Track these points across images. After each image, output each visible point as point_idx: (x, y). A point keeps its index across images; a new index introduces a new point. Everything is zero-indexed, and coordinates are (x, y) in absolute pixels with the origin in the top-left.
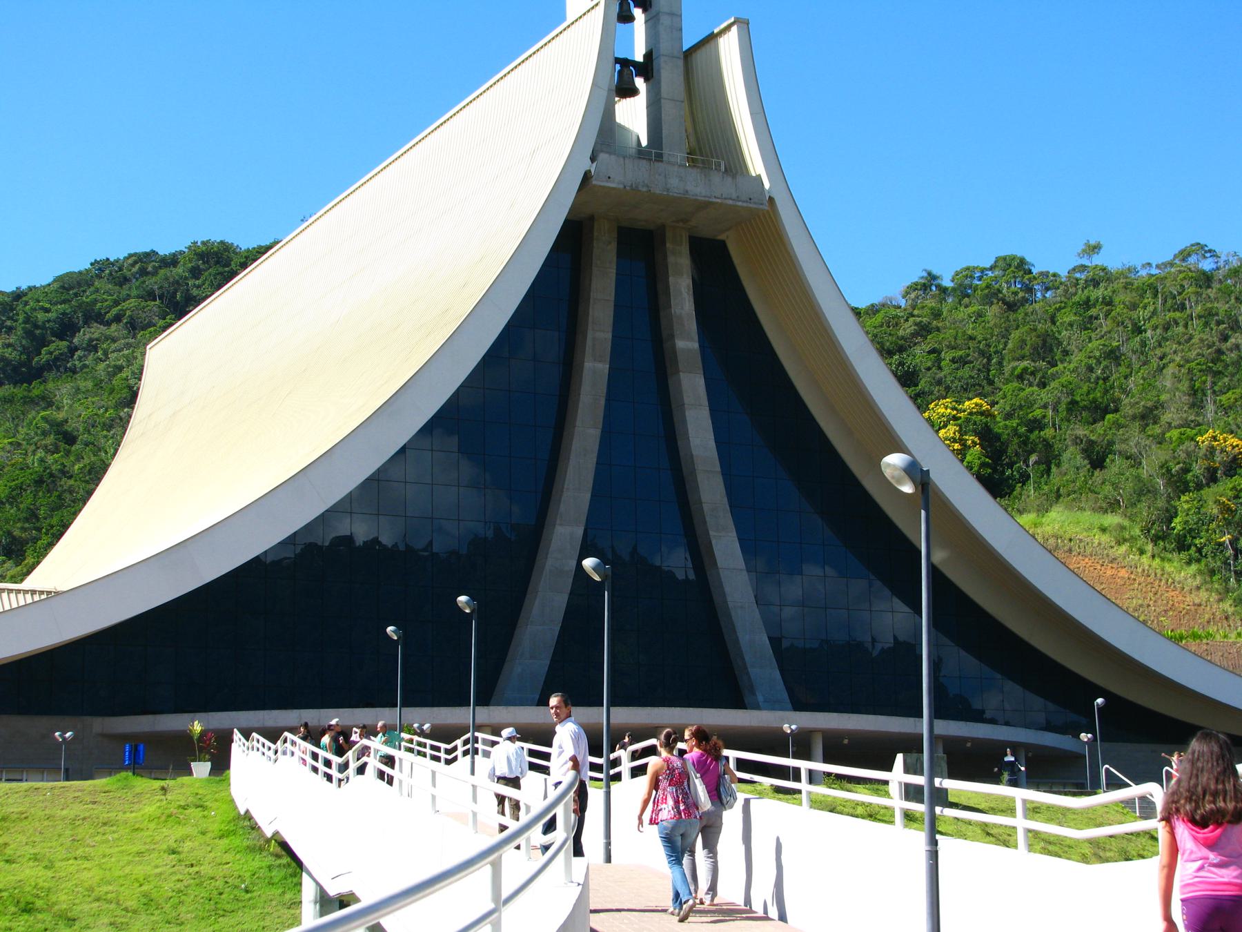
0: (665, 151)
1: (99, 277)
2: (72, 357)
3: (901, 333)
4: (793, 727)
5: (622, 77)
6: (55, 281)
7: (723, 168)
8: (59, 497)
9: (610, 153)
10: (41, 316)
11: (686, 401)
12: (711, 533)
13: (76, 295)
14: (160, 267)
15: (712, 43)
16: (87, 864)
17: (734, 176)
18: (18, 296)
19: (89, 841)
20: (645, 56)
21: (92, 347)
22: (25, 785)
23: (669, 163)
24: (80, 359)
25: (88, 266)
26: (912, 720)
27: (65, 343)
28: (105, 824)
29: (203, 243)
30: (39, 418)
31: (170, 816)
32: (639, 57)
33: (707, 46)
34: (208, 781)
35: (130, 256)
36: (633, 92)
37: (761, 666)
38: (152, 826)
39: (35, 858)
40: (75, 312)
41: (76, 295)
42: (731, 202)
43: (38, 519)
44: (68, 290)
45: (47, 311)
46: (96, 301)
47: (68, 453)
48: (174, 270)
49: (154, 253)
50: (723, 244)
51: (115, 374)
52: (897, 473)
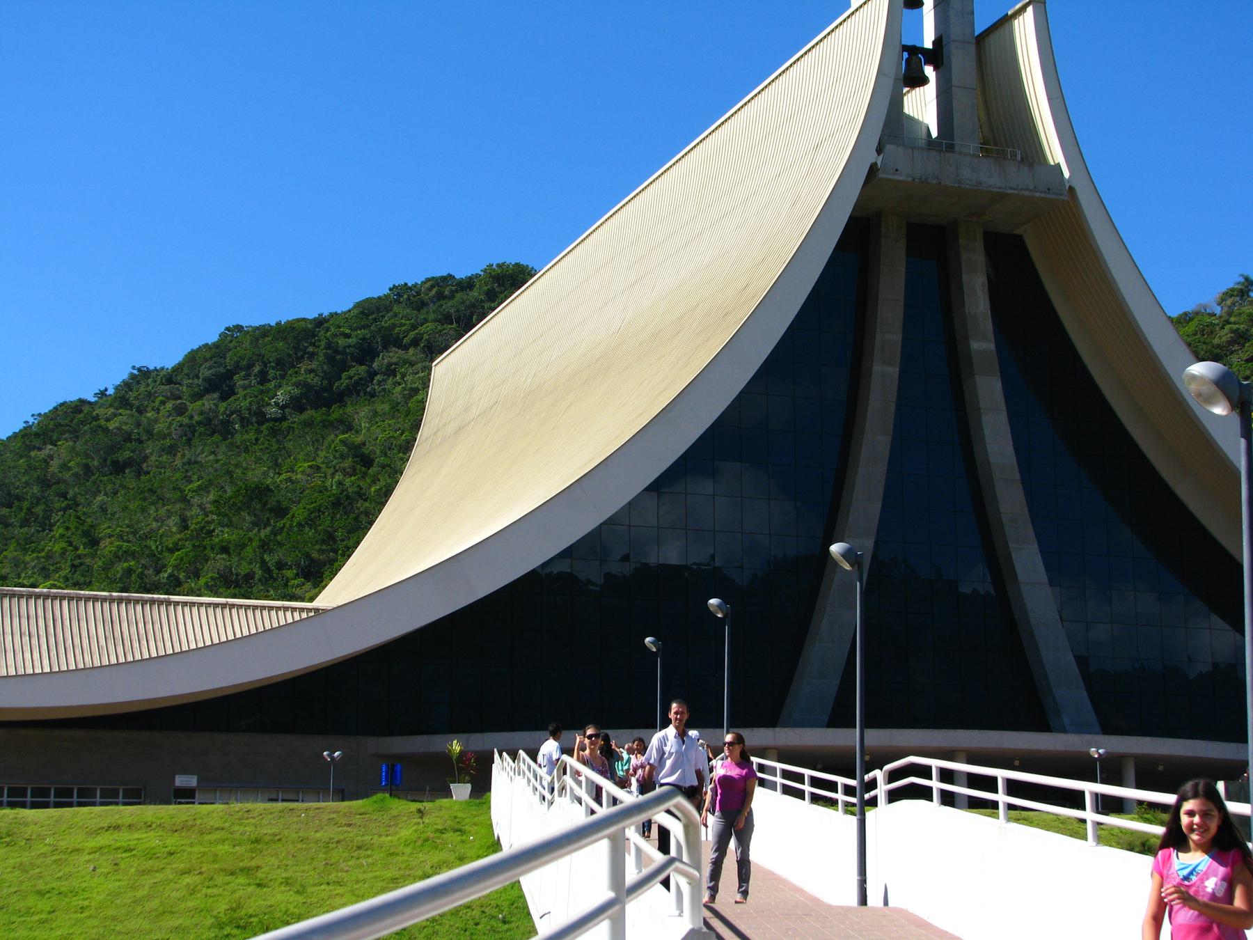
0: (957, 142)
1: (397, 302)
2: (372, 380)
3: (1216, 341)
4: (1101, 751)
5: (906, 65)
6: (355, 307)
7: (1019, 158)
8: (357, 519)
9: (898, 145)
10: (341, 342)
11: (982, 405)
12: (1010, 545)
13: (375, 320)
14: (457, 291)
15: (1007, 25)
16: (339, 890)
17: (1031, 166)
18: (320, 322)
19: (342, 865)
20: (934, 43)
21: (390, 371)
22: (280, 805)
23: (960, 153)
24: (379, 383)
25: (387, 291)
26: (1234, 745)
27: (363, 367)
28: (359, 848)
29: (498, 265)
30: (337, 441)
31: (426, 840)
32: (928, 43)
33: (1001, 29)
34: (467, 803)
35: (428, 280)
36: (923, 81)
37: (1067, 689)
38: (408, 850)
39: (287, 882)
40: (374, 337)
41: (375, 320)
42: (1027, 193)
43: (335, 542)
44: (368, 315)
45: (348, 336)
46: (394, 325)
47: (364, 475)
48: (471, 294)
49: (450, 276)
50: (1019, 240)
51: (411, 397)
52: (1205, 389)
